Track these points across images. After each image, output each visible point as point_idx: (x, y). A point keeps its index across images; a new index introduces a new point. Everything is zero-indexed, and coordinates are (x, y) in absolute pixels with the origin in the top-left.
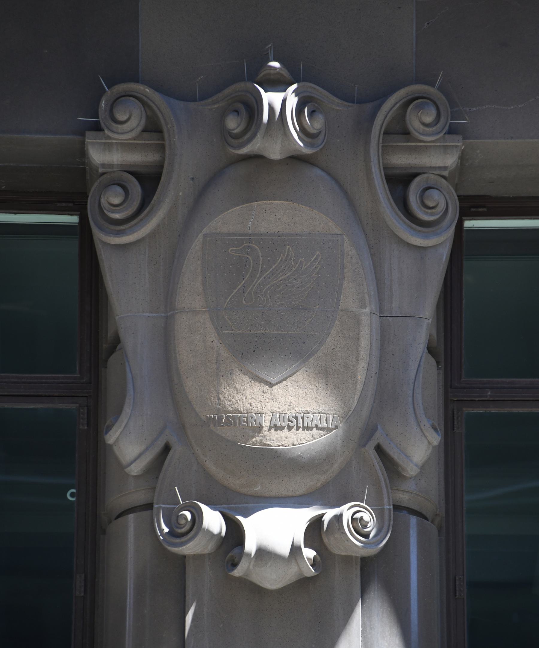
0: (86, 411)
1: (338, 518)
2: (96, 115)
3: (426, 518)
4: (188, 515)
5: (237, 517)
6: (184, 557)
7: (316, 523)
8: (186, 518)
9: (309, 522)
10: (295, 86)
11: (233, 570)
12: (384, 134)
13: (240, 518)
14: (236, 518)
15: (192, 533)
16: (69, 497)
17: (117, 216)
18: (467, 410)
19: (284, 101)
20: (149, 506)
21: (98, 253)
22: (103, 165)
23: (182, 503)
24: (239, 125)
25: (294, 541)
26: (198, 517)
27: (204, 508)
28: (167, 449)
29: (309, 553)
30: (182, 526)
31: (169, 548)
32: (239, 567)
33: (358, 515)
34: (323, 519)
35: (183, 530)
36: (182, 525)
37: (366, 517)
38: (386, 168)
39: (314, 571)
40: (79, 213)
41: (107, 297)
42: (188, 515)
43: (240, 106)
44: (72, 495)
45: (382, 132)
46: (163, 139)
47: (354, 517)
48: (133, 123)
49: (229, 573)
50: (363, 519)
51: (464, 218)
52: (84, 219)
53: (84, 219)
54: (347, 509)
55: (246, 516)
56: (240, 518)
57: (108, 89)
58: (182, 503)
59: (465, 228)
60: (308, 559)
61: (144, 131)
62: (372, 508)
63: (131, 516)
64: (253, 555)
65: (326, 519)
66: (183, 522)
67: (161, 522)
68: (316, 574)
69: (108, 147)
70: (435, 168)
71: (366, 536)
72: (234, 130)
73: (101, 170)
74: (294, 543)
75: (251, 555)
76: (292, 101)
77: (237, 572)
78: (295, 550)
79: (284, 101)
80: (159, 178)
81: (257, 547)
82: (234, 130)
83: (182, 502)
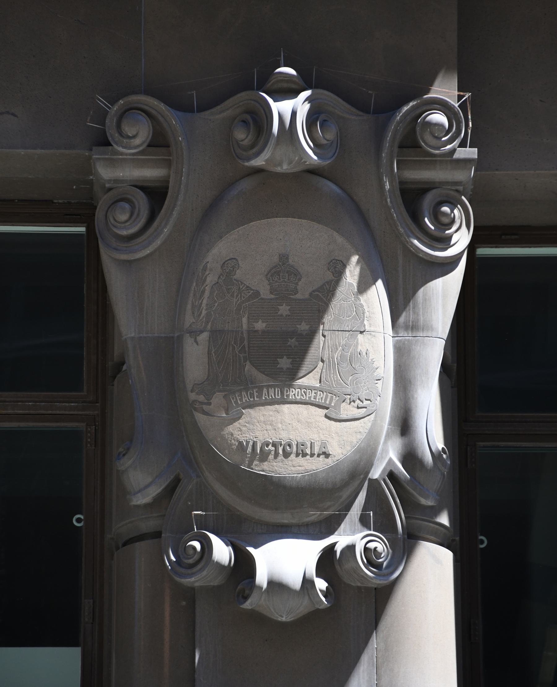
0: (93, 431)
1: (351, 548)
2: (103, 124)
4: (197, 545)
5: (247, 548)
6: (193, 589)
7: (329, 551)
8: (194, 548)
9: (458, 112)
10: (307, 93)
11: (245, 602)
12: (401, 147)
13: (250, 549)
14: (247, 549)
15: (199, 567)
16: (75, 523)
17: (124, 233)
19: (294, 114)
20: (157, 535)
21: (105, 271)
22: (109, 181)
23: (196, 531)
24: (247, 137)
25: (306, 573)
26: (207, 546)
27: (213, 537)
29: (321, 584)
30: (192, 556)
31: (177, 579)
32: (249, 601)
33: (371, 545)
34: (335, 549)
35: (191, 561)
36: (189, 555)
37: (380, 547)
38: (401, 183)
39: (326, 603)
40: (85, 225)
41: (113, 317)
42: (197, 545)
43: (248, 117)
44: (79, 520)
45: (396, 144)
46: (170, 154)
47: (367, 546)
48: (137, 141)
49: (240, 605)
50: (377, 550)
51: (476, 246)
52: (91, 229)
53: (91, 229)
54: (361, 538)
55: (256, 547)
56: (250, 549)
57: (110, 110)
58: (196, 531)
59: (477, 256)
60: (321, 591)
61: (149, 146)
62: (387, 537)
63: (140, 546)
64: (264, 589)
65: (339, 549)
66: (191, 552)
67: (170, 555)
68: (329, 606)
69: (112, 163)
70: (447, 183)
71: (378, 566)
72: (242, 141)
73: (107, 185)
74: (307, 575)
75: (262, 588)
76: (303, 110)
77: (247, 605)
78: (307, 583)
79: (294, 114)
80: (166, 193)
81: (268, 577)
82: (242, 141)
83: (197, 530)
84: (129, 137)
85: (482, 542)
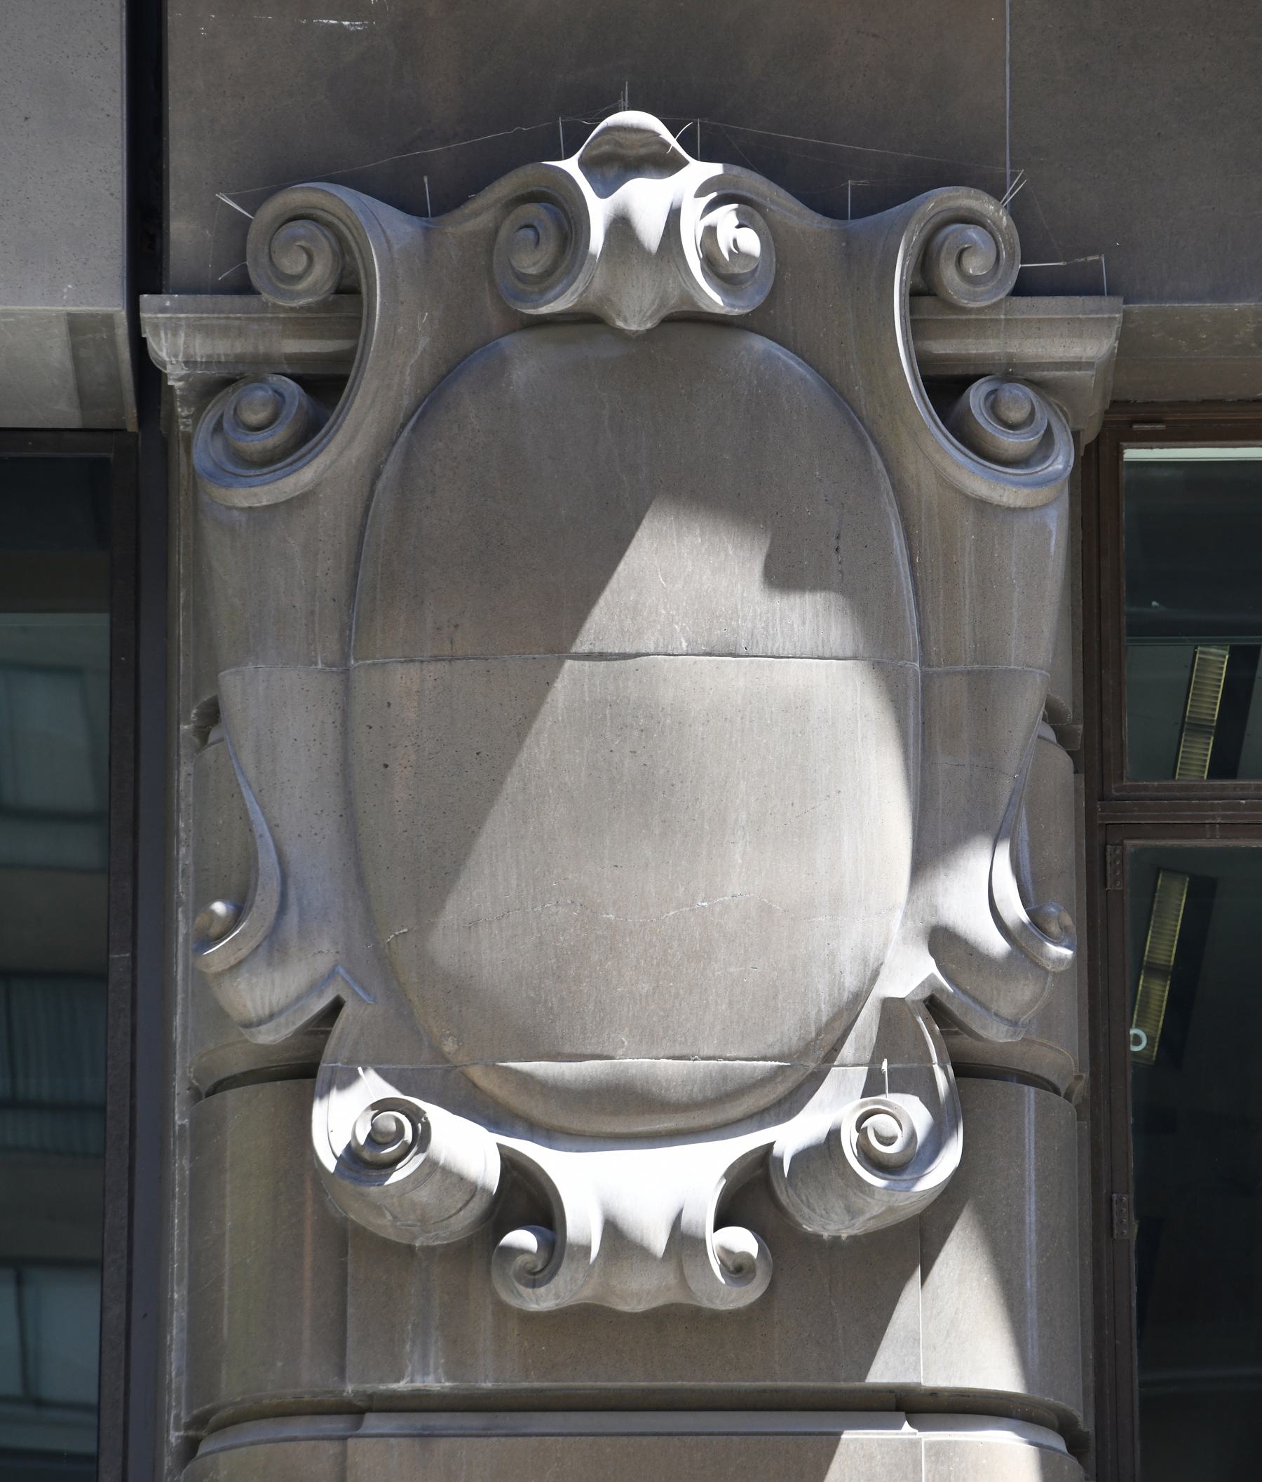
3: (1056, 1091)
18: (1131, 844)
19: (674, 216)
28: (336, 1007)
51: (1125, 444)
79: (674, 216)
84: (299, 278)
85: (1137, 1040)
